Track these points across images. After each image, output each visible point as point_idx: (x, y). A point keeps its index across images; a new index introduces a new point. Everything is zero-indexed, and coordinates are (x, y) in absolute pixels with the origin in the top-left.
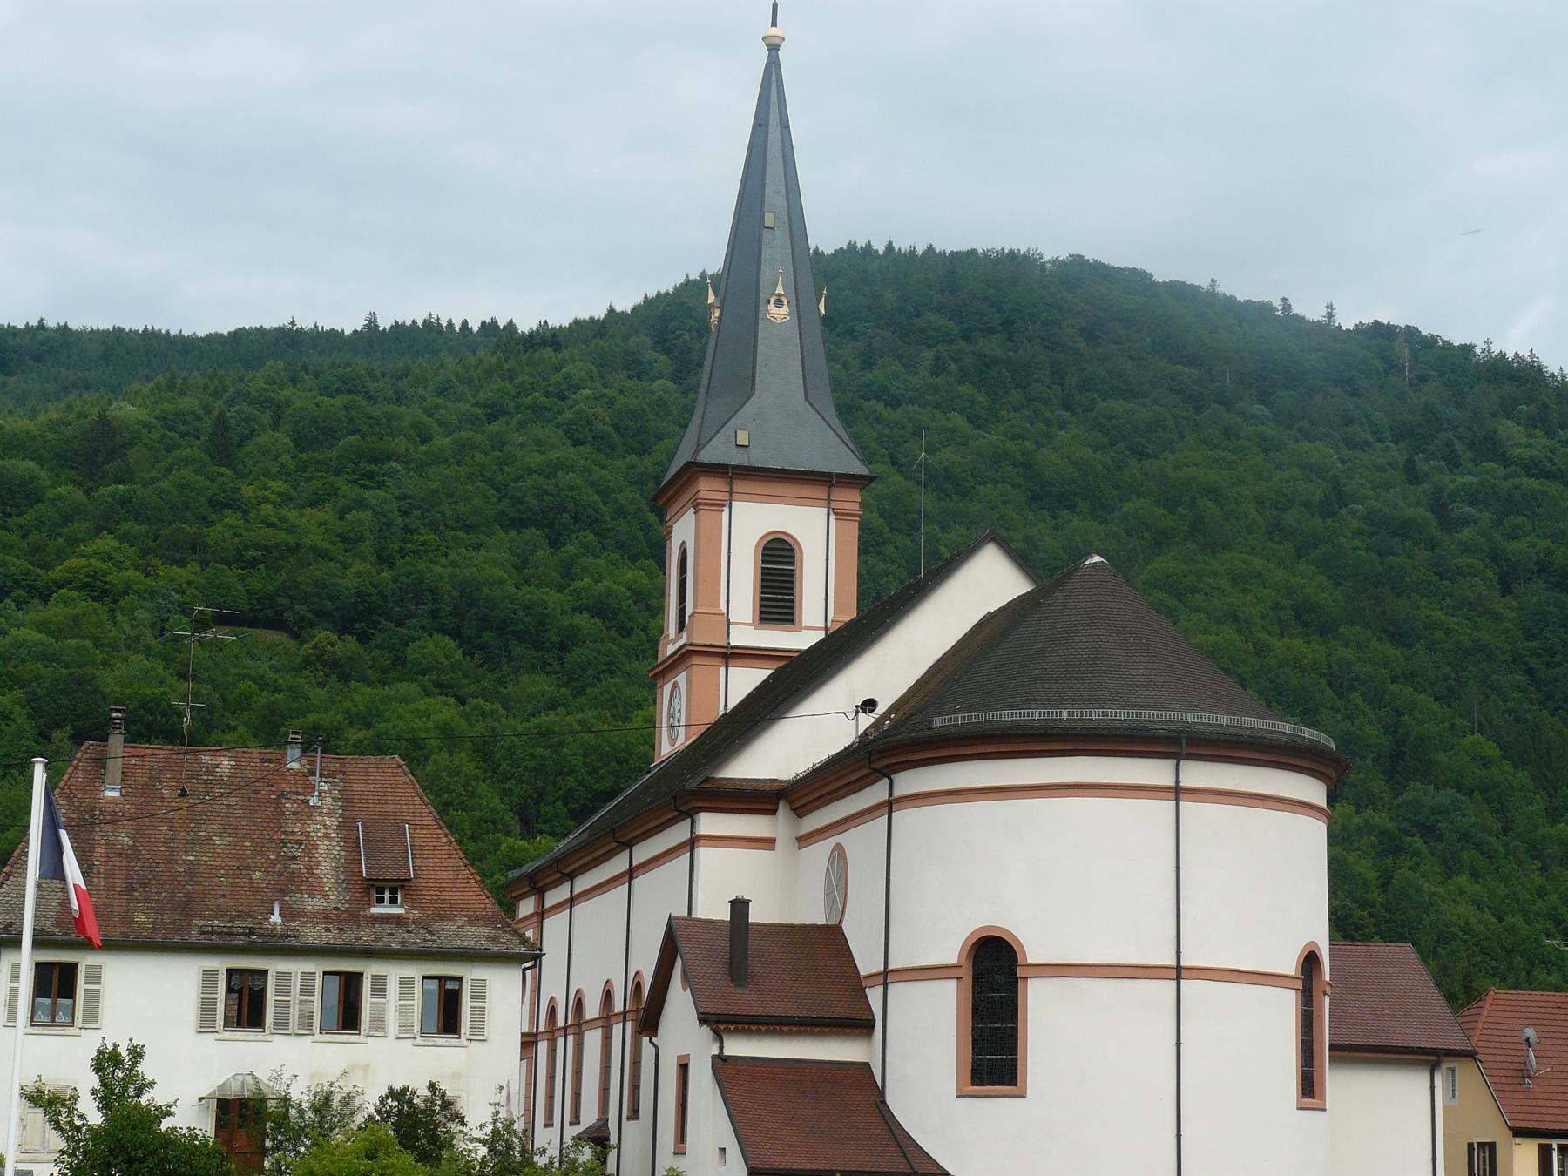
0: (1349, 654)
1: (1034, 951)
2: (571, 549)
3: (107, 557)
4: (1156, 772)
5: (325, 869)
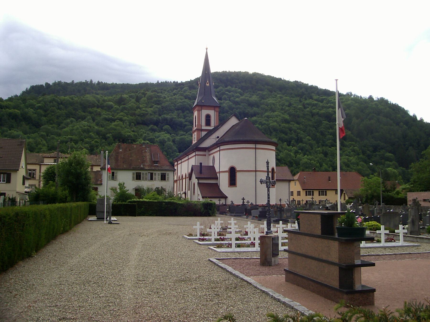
0: (292, 126)
1: (238, 169)
2: (185, 113)
3: (122, 116)
4: (253, 146)
5: (148, 159)
